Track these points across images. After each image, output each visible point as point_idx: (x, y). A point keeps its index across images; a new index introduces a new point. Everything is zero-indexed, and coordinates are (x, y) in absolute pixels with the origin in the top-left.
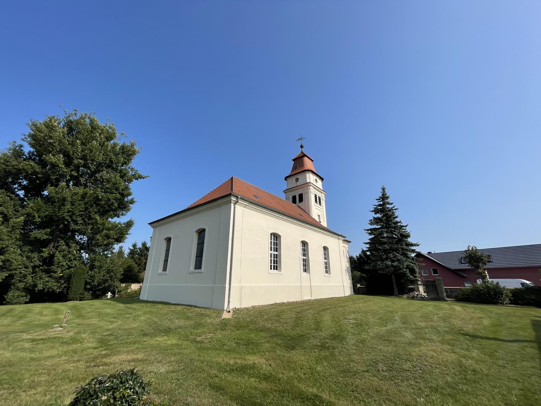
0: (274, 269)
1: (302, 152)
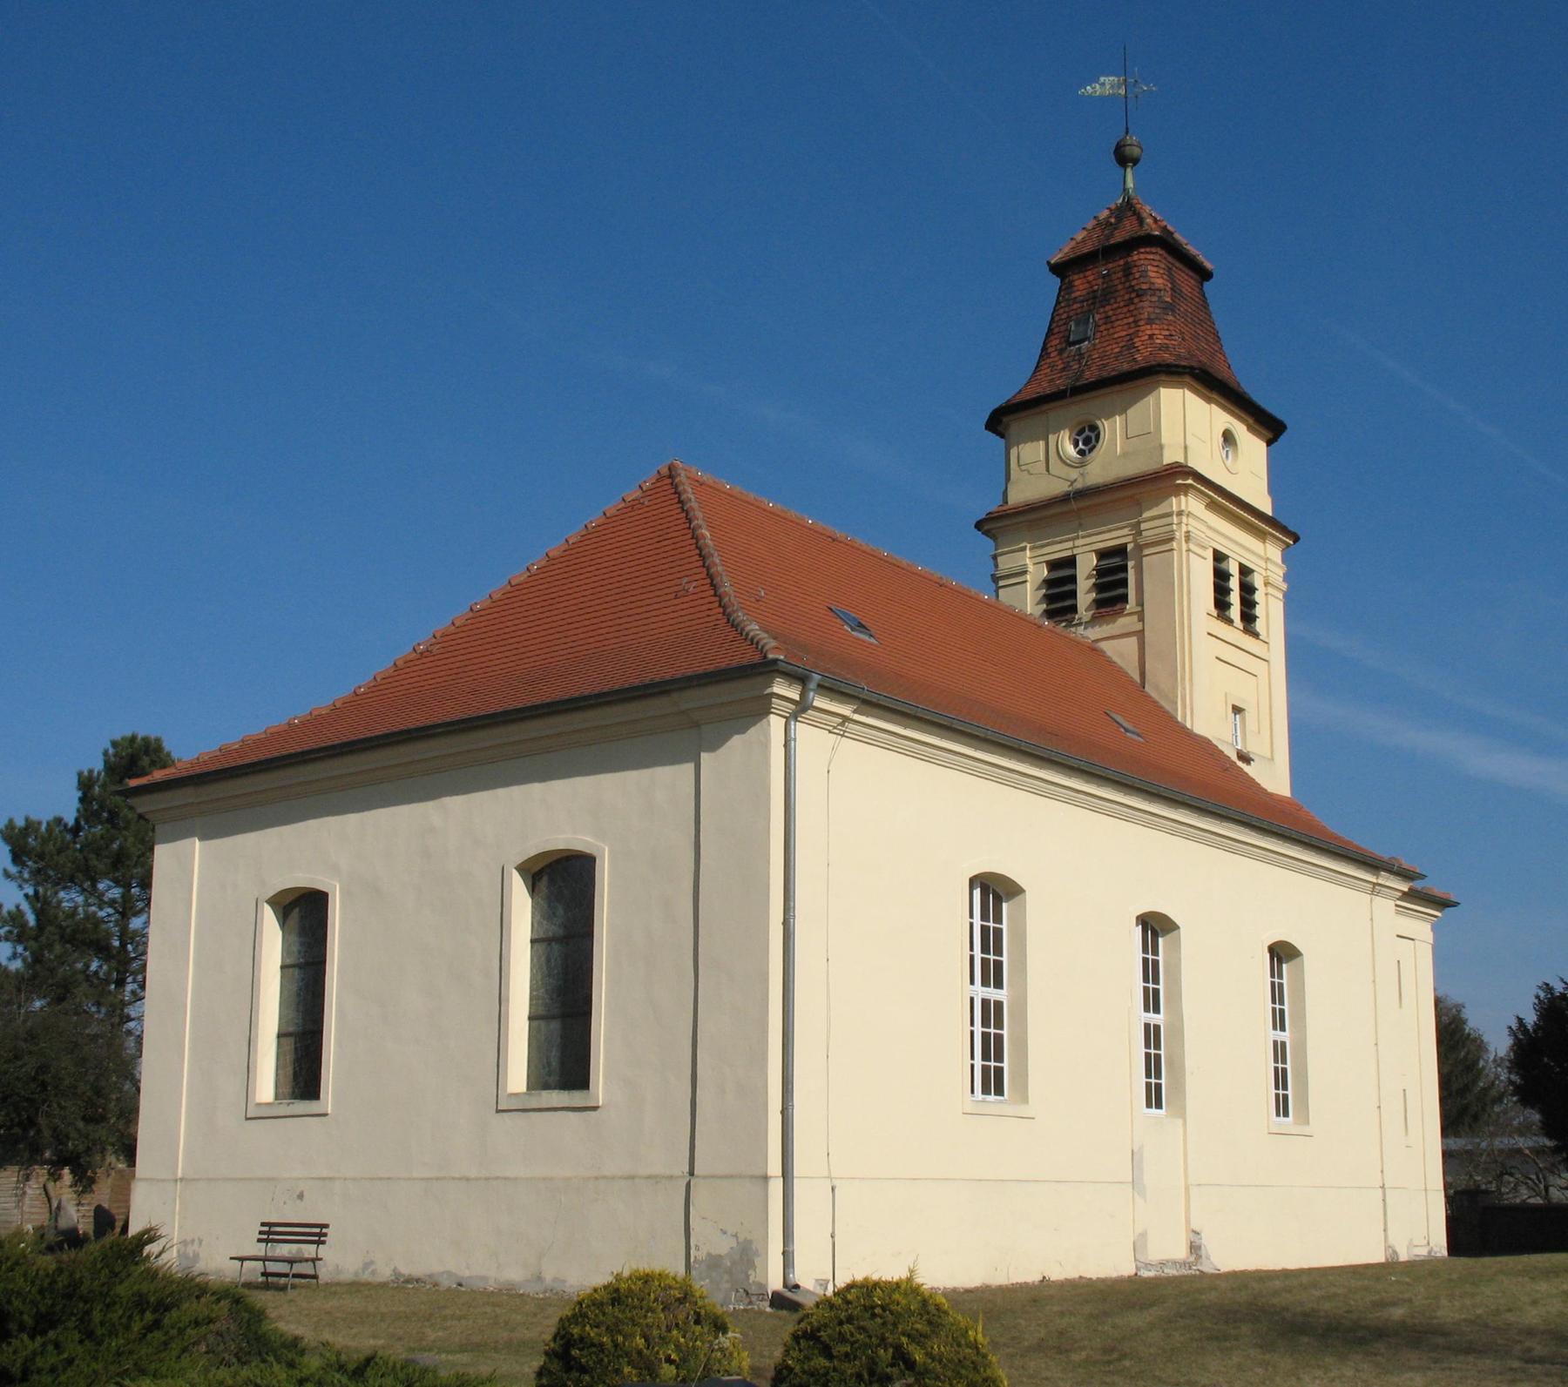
0: (986, 1091)
1: (1128, 208)
